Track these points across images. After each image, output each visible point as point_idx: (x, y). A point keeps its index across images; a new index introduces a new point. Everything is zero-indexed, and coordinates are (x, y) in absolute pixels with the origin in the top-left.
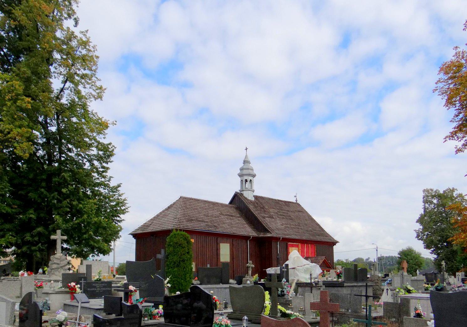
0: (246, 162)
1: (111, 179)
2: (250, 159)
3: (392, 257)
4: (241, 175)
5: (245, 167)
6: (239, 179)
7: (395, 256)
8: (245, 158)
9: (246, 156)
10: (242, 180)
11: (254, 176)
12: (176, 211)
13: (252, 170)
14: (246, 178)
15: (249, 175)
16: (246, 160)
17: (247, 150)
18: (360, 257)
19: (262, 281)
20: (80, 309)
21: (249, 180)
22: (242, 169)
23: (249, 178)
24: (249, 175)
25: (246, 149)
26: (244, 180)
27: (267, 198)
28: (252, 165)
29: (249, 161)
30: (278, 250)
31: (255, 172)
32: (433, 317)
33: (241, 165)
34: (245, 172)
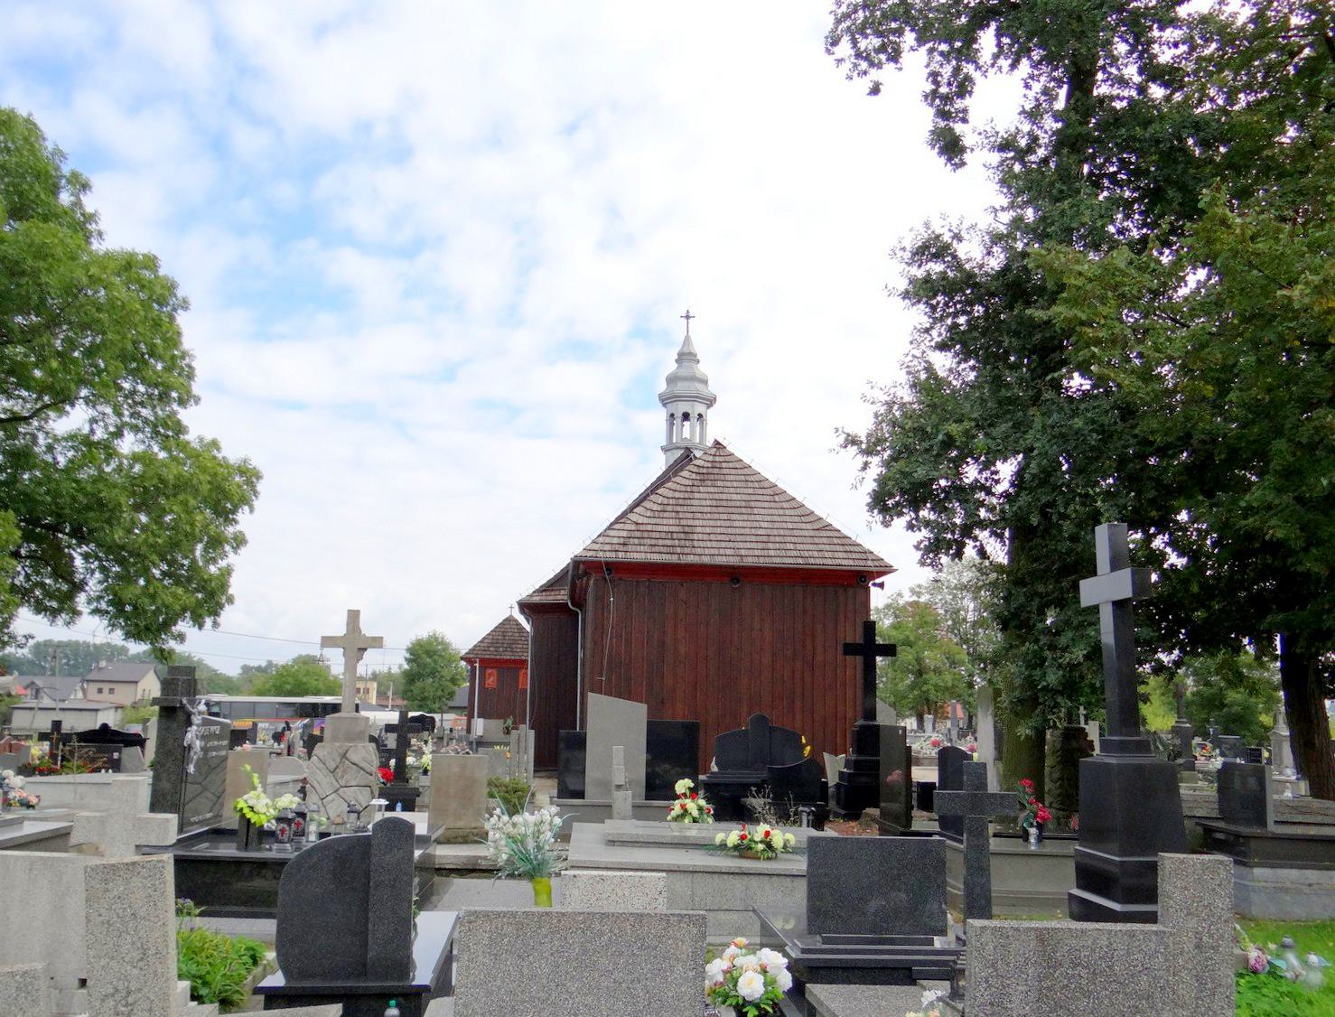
0: (686, 357)
1: (933, 993)
2: (698, 347)
3: (77, 643)
4: (665, 400)
5: (683, 372)
6: (661, 415)
7: (84, 642)
8: (683, 346)
9: (687, 340)
10: (672, 415)
11: (710, 402)
12: (683, 489)
13: (705, 382)
14: (682, 407)
15: (695, 398)
16: (686, 350)
17: (691, 320)
18: (304, 654)
19: (125, 462)
20: (127, 771)
21: (694, 415)
22: (671, 380)
23: (700, 408)
24: (695, 398)
25: (688, 317)
26: (679, 415)
27: (348, 624)
28: (703, 368)
29: (695, 356)
30: (525, 710)
31: (713, 388)
32: (498, 721)
33: (672, 367)
34: (681, 388)
